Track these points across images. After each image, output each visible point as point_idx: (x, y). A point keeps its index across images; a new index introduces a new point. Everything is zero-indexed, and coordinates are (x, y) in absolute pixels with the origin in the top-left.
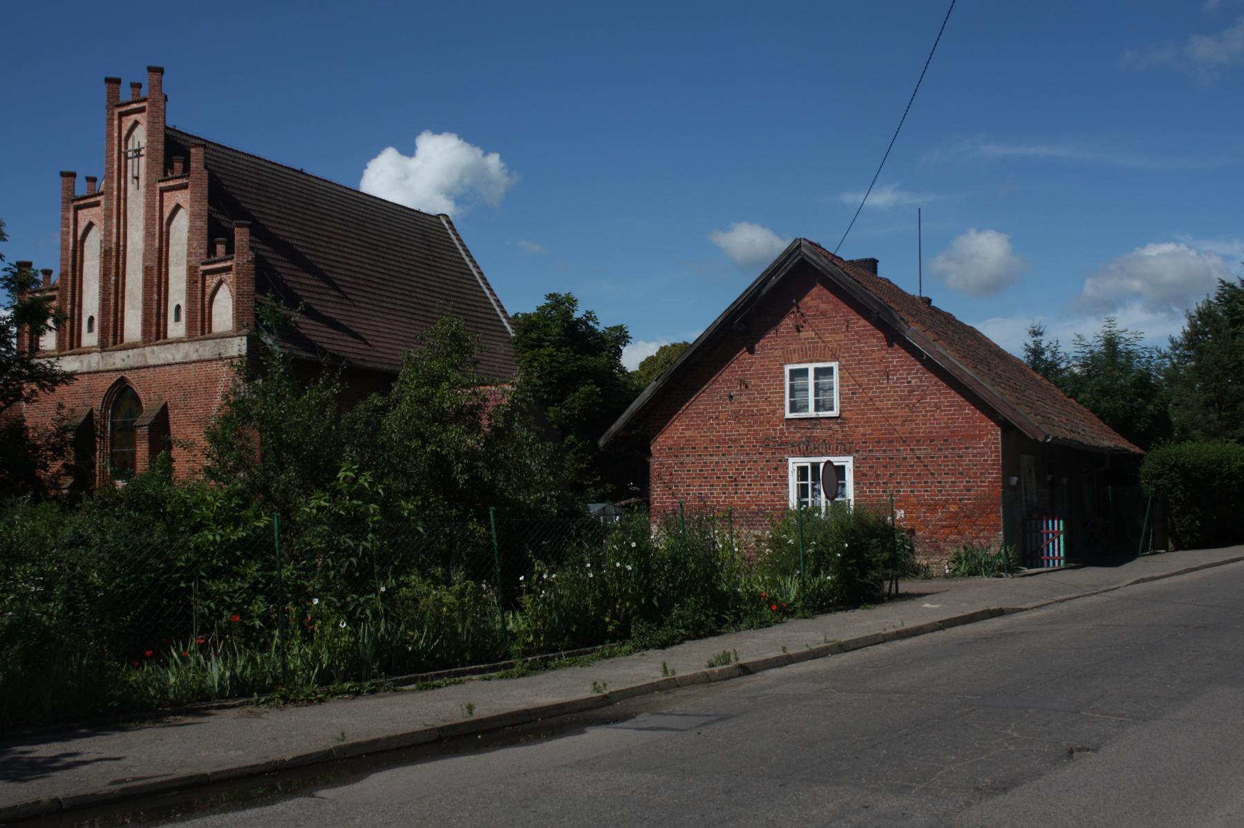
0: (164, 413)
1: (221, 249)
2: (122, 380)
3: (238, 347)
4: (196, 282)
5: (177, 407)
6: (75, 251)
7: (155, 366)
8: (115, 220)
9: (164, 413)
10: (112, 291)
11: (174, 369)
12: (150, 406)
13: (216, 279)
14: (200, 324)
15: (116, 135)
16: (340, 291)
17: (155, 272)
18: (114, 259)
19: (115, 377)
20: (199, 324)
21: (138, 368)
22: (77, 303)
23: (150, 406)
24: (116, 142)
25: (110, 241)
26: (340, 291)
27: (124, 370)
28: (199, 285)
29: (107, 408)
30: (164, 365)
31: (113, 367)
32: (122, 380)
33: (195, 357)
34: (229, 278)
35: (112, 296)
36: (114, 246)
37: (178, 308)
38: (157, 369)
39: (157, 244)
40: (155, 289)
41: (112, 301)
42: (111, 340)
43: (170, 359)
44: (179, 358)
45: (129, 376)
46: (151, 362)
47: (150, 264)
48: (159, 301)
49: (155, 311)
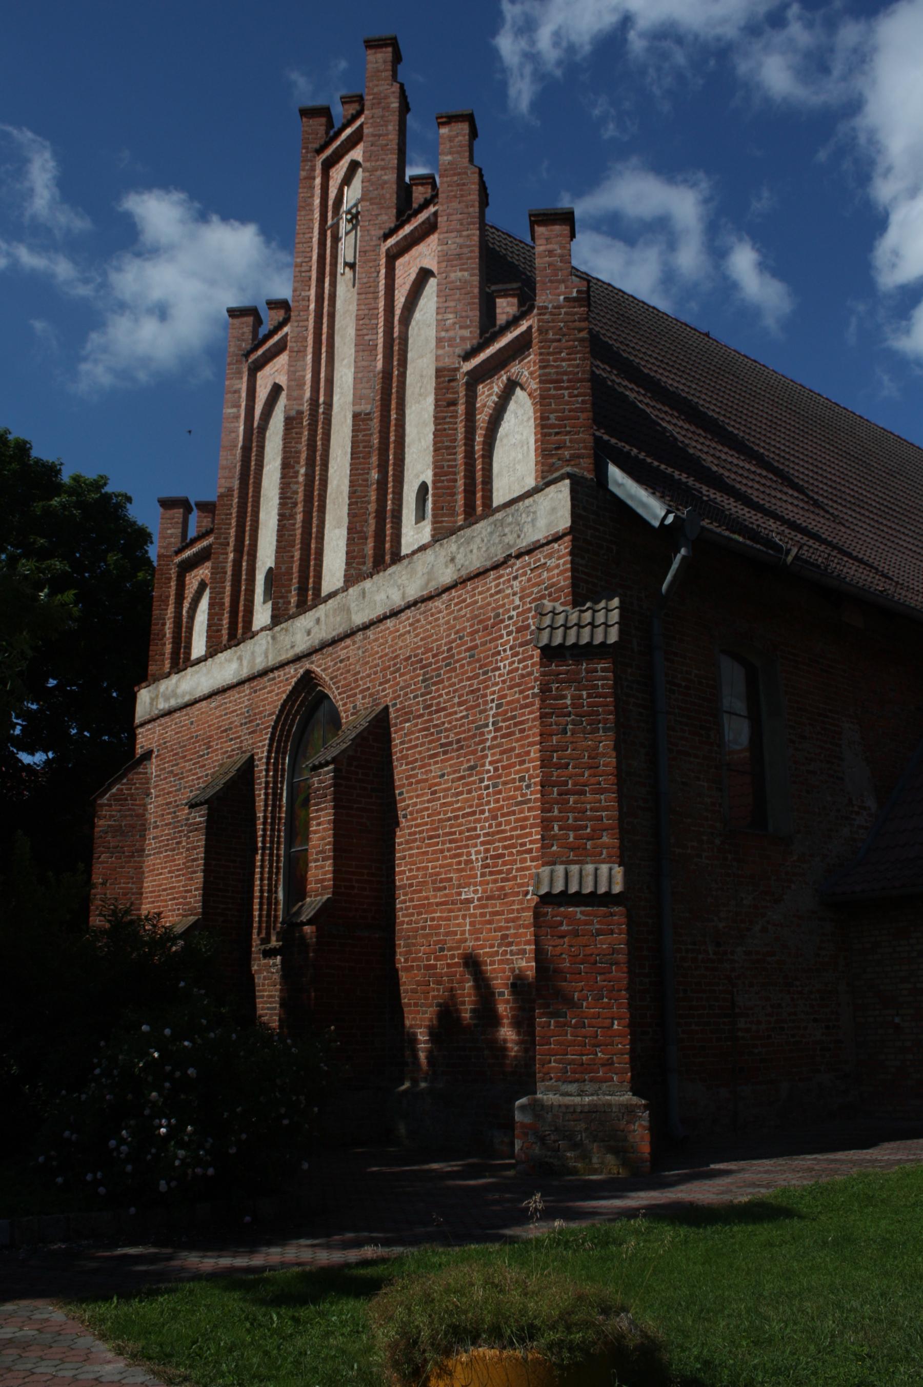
0: (379, 729)
1: (505, 307)
2: (308, 681)
3: (554, 510)
4: (453, 403)
5: (407, 714)
6: (247, 449)
7: (366, 627)
8: (309, 357)
9: (379, 729)
10: (300, 497)
11: (402, 624)
12: (353, 710)
13: (497, 385)
14: (466, 493)
15: (317, 201)
16: (807, 495)
17: (375, 424)
18: (309, 431)
19: (294, 673)
20: (460, 499)
21: (334, 642)
22: (246, 549)
23: (353, 710)
24: (317, 215)
25: (300, 398)
26: (807, 495)
27: (307, 655)
28: (461, 409)
29: (281, 752)
30: (384, 618)
31: (290, 654)
32: (308, 681)
33: (447, 576)
34: (525, 369)
35: (300, 508)
36: (306, 407)
37: (423, 487)
38: (370, 633)
39: (380, 365)
40: (374, 459)
41: (299, 517)
42: (293, 600)
43: (397, 600)
44: (413, 591)
45: (316, 666)
46: (359, 619)
47: (365, 407)
48: (382, 484)
49: (372, 507)
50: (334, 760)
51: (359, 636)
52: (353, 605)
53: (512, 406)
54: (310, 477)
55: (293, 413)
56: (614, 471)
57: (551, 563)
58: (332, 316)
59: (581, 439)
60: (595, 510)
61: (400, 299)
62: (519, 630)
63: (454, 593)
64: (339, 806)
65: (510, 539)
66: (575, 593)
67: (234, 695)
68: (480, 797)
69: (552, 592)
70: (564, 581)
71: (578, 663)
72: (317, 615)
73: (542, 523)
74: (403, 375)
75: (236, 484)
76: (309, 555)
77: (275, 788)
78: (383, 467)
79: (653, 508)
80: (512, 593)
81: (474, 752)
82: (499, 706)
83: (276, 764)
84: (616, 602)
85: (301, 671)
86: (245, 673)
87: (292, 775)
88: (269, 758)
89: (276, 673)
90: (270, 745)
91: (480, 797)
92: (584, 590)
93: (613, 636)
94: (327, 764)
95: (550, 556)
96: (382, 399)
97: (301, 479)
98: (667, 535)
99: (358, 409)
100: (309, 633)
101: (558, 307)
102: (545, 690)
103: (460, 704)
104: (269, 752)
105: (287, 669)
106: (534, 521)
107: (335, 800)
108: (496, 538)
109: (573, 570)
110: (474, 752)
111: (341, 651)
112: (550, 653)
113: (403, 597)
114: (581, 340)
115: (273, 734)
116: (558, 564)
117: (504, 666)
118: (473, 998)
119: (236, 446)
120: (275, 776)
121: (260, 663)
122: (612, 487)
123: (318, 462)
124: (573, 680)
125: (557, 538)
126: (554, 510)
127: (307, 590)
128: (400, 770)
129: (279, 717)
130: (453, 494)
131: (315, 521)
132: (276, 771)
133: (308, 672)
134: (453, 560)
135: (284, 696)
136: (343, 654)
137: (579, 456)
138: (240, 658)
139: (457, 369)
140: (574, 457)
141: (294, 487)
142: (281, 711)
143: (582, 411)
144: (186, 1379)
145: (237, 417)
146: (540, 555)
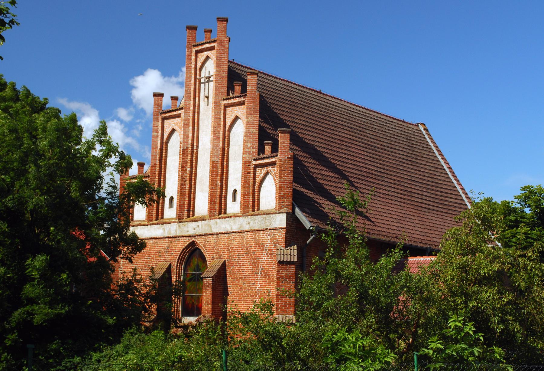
0: (223, 269)
3: (281, 221)
5: (232, 264)
6: (161, 150)
8: (191, 128)
11: (232, 236)
13: (264, 170)
17: (219, 166)
18: (190, 156)
19: (188, 241)
20: (251, 204)
28: (252, 175)
29: (181, 263)
32: (193, 243)
33: (247, 228)
34: (274, 170)
36: (189, 146)
38: (219, 236)
40: (219, 178)
44: (235, 229)
46: (215, 231)
47: (215, 159)
49: (218, 193)
50: (212, 277)
51: (215, 236)
52: (212, 226)
53: (267, 178)
54: (191, 172)
55: (185, 148)
56: (297, 210)
57: (280, 234)
58: (199, 113)
59: (289, 200)
60: (293, 222)
61: (228, 124)
62: (269, 250)
63: (249, 233)
64: (214, 289)
65: (268, 224)
66: (286, 244)
67: (162, 241)
68: (256, 292)
69: (279, 242)
70: (283, 240)
71: (287, 265)
72: (198, 224)
73: (277, 223)
74: (228, 149)
75: (157, 162)
76: (191, 199)
77: (179, 275)
78: (222, 181)
79: (307, 224)
80: (267, 239)
81: (254, 280)
82: (262, 269)
83: (179, 267)
84: (295, 247)
85: (191, 241)
86: (166, 235)
87: (184, 271)
88: (177, 265)
89: (180, 239)
90: (178, 261)
91: (256, 292)
92: (288, 244)
93: (296, 260)
94: (210, 277)
95: (279, 232)
96: (222, 157)
97: (188, 172)
98: (310, 232)
99: (213, 159)
100: (194, 229)
101: (285, 160)
102: (278, 271)
103: (250, 265)
104: (177, 263)
105: (185, 238)
106: (275, 221)
107: (212, 288)
108: (263, 222)
109: (286, 238)
110: (254, 280)
111: (208, 238)
112: (280, 262)
113: (232, 229)
114: (291, 171)
115: (179, 258)
116: (281, 235)
117: (264, 259)
118: (47, 307)
119: (157, 148)
120: (179, 271)
121: (173, 234)
122: (296, 214)
123: (194, 167)
124: (285, 269)
125: (282, 228)
126: (281, 220)
127: (190, 211)
128: (229, 280)
129: (181, 253)
130: (249, 202)
131: (193, 188)
132: (179, 269)
133: (193, 242)
134: (249, 223)
135: (184, 247)
136: (208, 240)
137: (288, 205)
138: (164, 229)
139: (251, 162)
140: (287, 205)
141: (186, 174)
142: (182, 251)
143: (290, 192)
144: (366, 354)
145: (157, 136)
146: (276, 231)
